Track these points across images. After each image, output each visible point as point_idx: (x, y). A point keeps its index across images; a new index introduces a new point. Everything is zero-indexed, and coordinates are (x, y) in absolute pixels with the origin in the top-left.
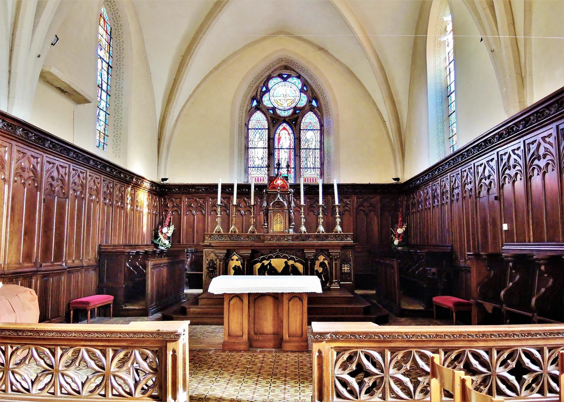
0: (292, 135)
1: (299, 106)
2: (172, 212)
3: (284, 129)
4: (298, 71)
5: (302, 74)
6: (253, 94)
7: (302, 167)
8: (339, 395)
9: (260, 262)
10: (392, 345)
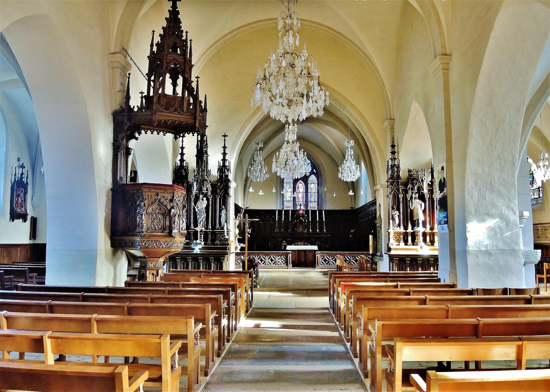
3: (300, 183)
8: (321, 264)
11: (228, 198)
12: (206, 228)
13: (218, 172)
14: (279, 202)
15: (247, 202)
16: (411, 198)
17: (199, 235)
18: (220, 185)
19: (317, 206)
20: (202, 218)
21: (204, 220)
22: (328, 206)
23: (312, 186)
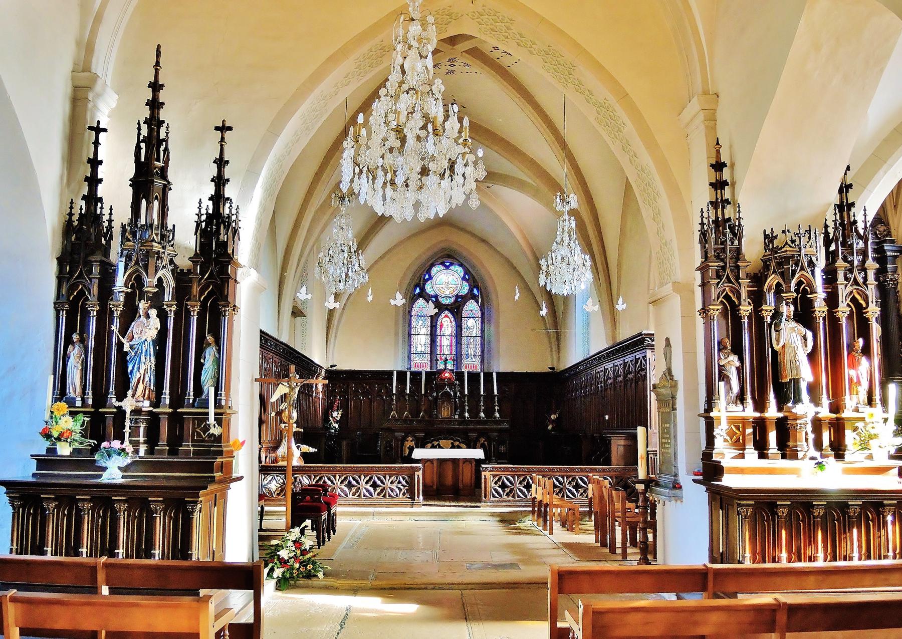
0: (454, 323)
1: (460, 294)
2: (340, 397)
3: (446, 316)
4: (460, 260)
5: (465, 264)
6: (416, 281)
7: (463, 354)
8: (494, 496)
9: (431, 443)
10: (519, 473)
11: (225, 311)
12: (156, 403)
13: (196, 234)
14: (400, 356)
15: (333, 354)
16: (777, 315)
17: (127, 424)
18: (203, 273)
19: (479, 363)
20: (142, 371)
21: (147, 379)
22: (504, 364)
23: (471, 322)
